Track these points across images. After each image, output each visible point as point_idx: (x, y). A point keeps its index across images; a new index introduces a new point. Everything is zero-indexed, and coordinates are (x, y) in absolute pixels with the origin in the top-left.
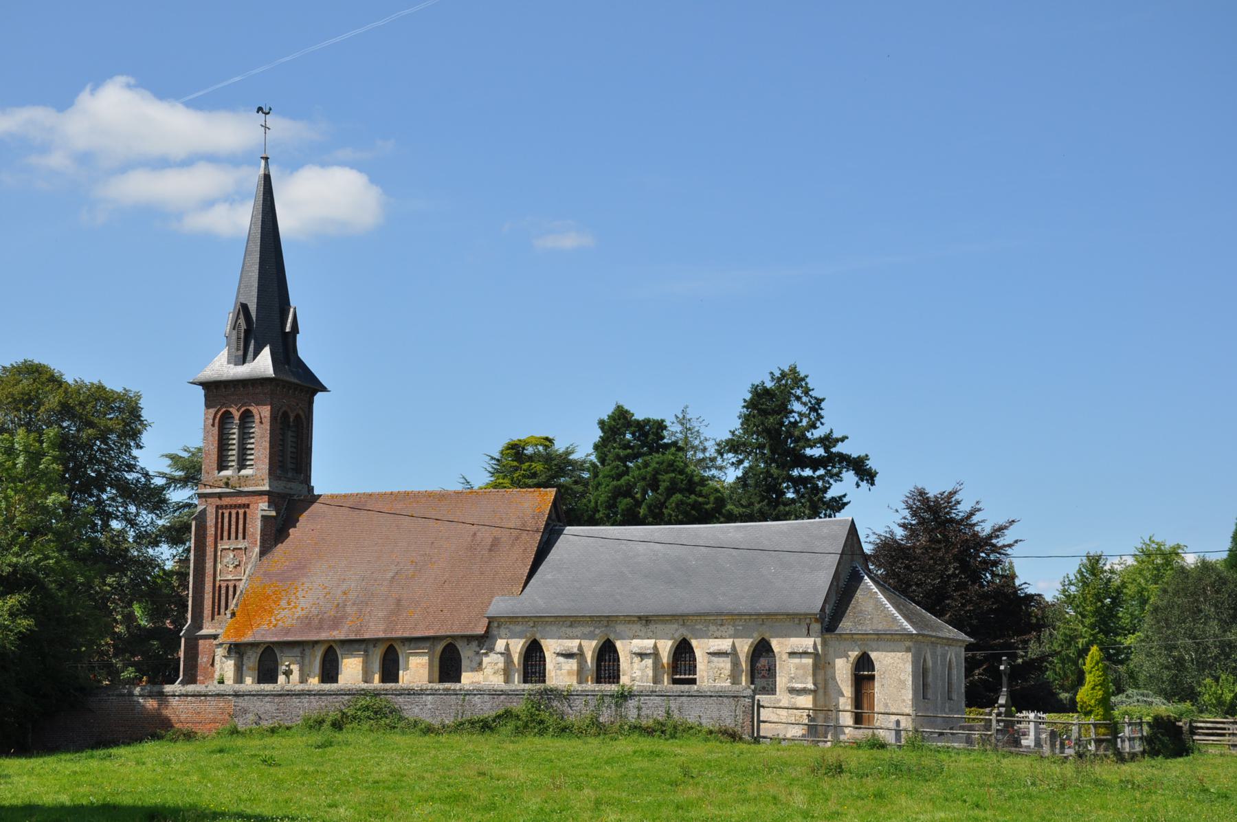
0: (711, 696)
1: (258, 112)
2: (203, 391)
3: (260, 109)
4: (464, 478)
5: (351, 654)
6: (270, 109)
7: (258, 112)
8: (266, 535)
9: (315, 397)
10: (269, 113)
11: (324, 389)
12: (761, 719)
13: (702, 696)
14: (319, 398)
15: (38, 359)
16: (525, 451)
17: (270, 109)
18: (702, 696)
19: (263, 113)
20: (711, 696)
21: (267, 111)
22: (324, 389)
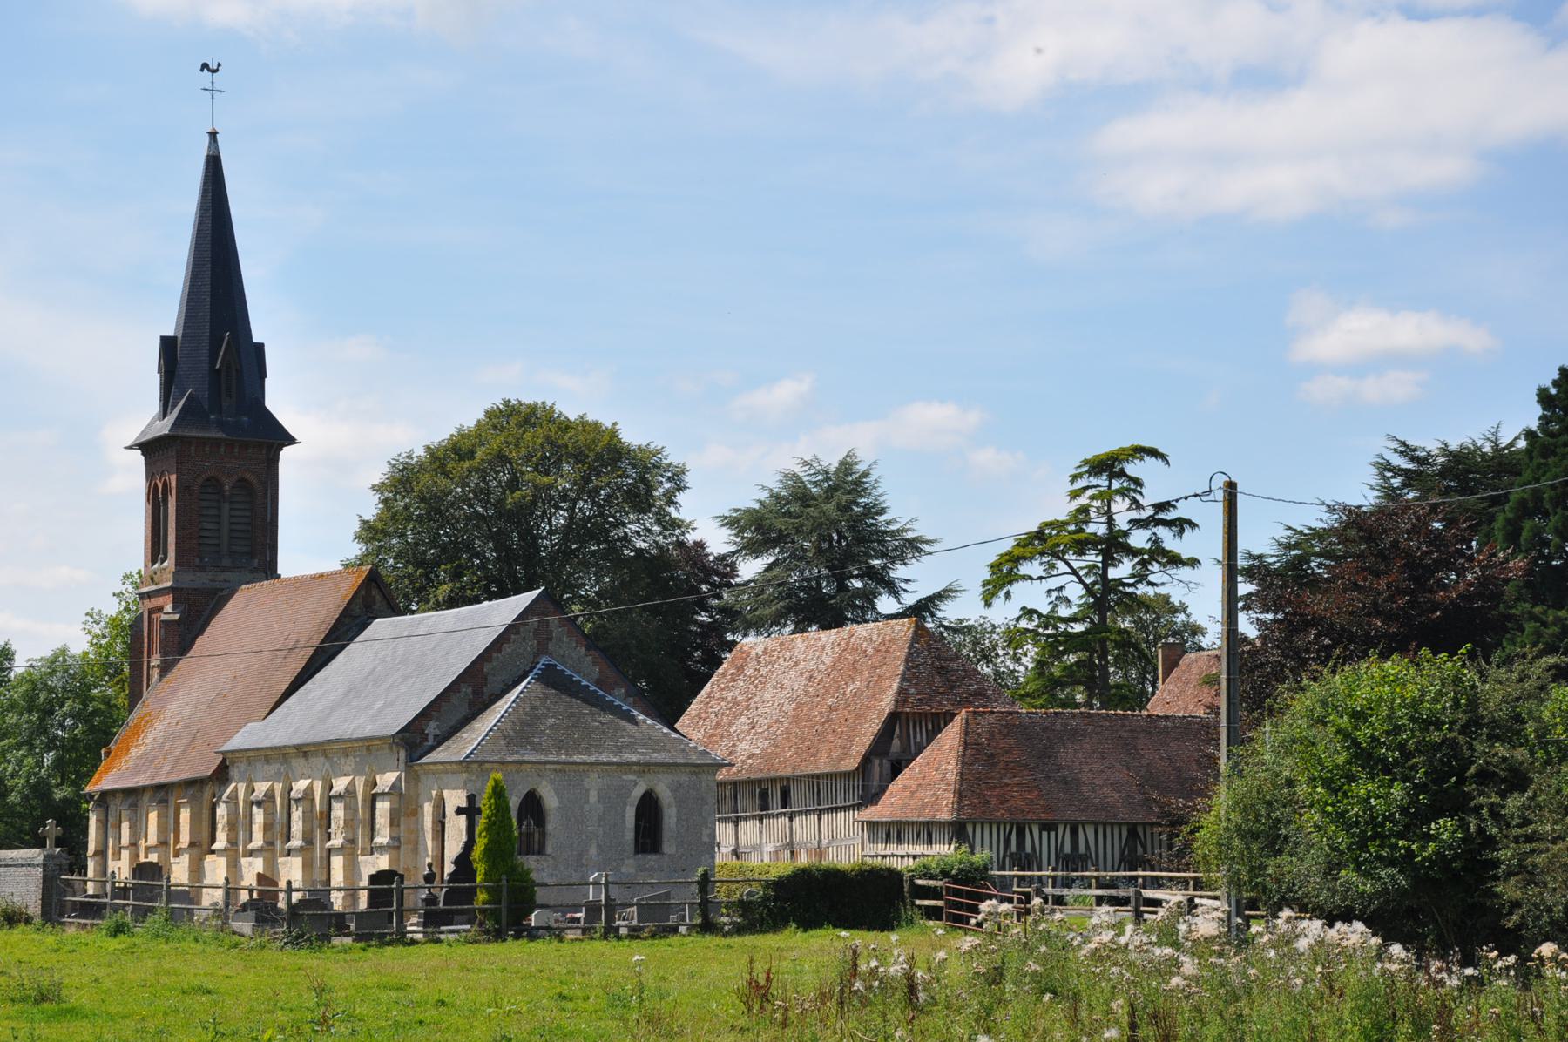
0: (22, 866)
1: (202, 70)
2: (143, 458)
3: (205, 66)
4: (1290, 528)
5: (184, 807)
6: (219, 65)
7: (202, 70)
8: (167, 646)
9: (281, 453)
10: (217, 71)
11: (291, 441)
12: (406, 906)
13: (14, 866)
14: (286, 454)
15: (528, 395)
16: (671, 510)
17: (219, 65)
18: (14, 866)
19: (209, 70)
20: (22, 866)
21: (215, 68)
22: (291, 441)
